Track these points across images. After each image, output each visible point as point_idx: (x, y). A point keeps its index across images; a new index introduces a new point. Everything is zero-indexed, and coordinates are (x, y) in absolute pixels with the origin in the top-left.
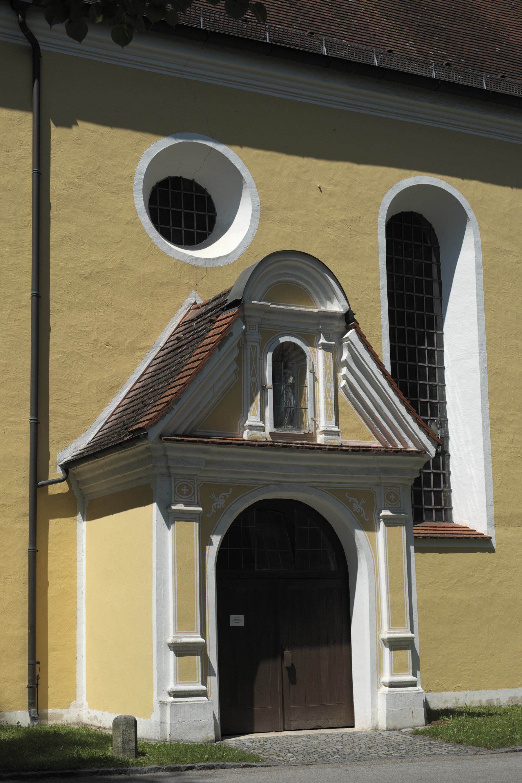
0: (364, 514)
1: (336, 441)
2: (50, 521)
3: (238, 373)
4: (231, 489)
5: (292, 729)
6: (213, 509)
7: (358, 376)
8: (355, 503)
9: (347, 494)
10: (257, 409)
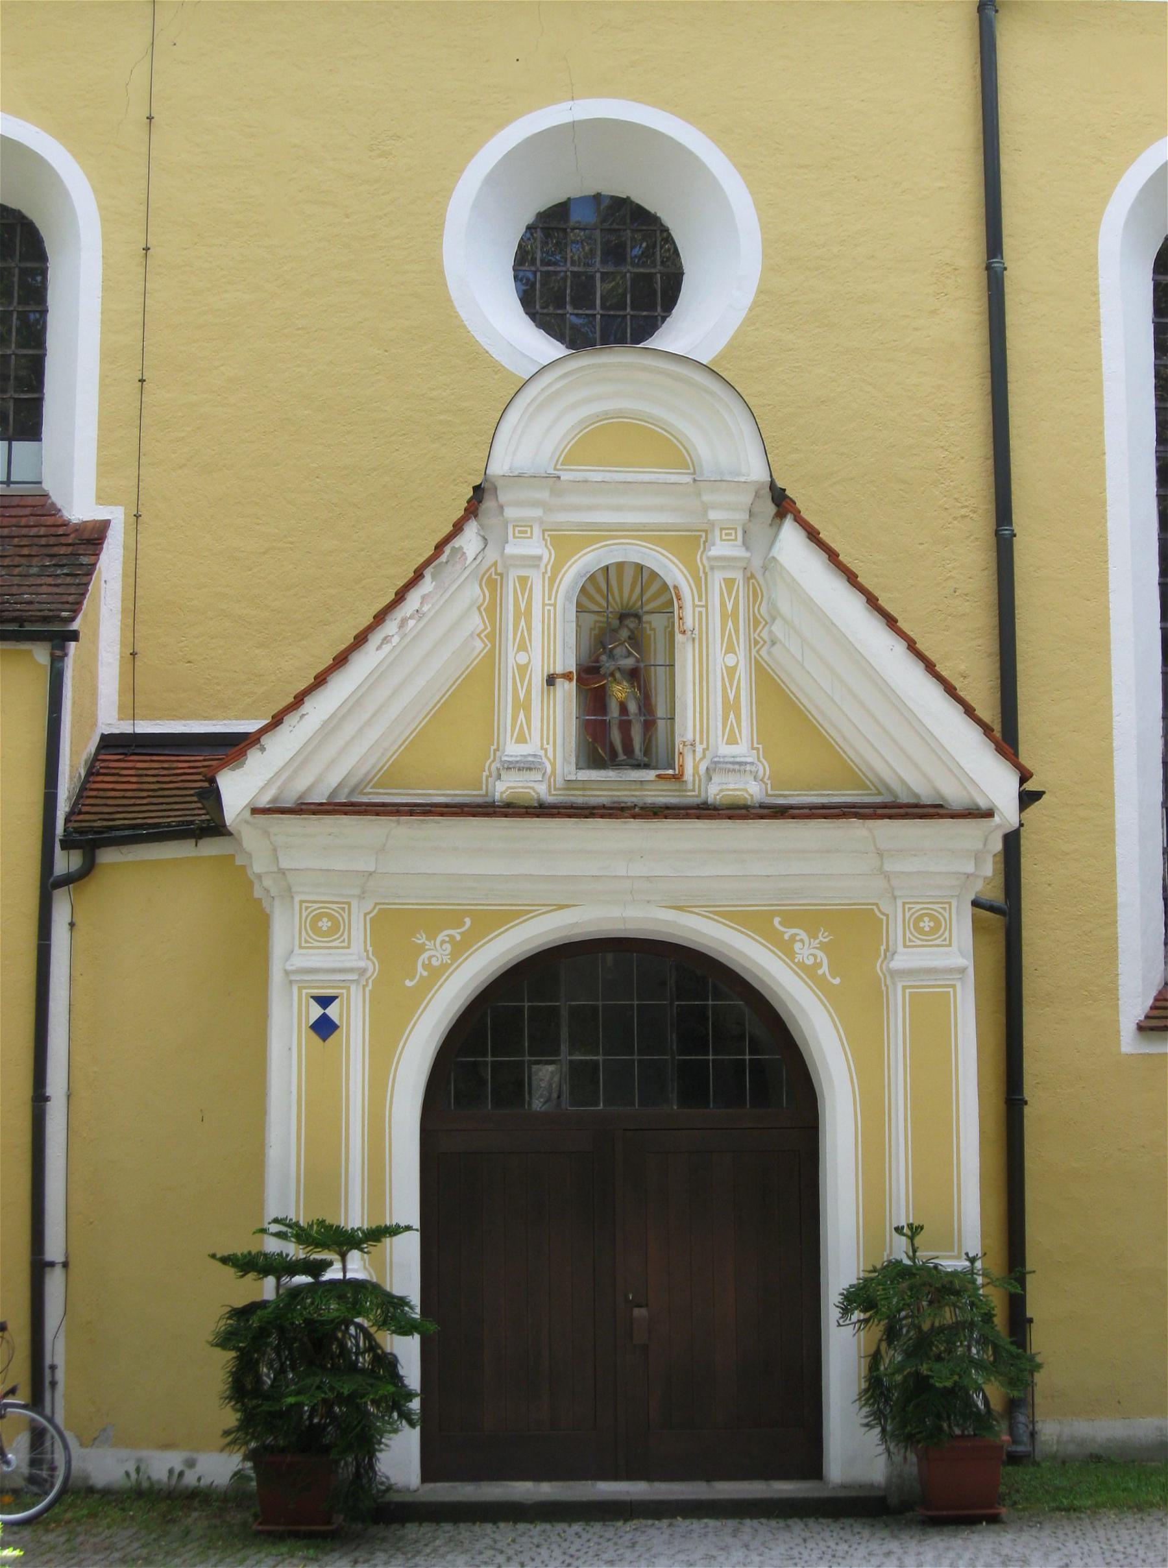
0: (824, 969)
3: (494, 636)
4: (468, 921)
7: (94, 676)
8: (802, 941)
9: (777, 920)
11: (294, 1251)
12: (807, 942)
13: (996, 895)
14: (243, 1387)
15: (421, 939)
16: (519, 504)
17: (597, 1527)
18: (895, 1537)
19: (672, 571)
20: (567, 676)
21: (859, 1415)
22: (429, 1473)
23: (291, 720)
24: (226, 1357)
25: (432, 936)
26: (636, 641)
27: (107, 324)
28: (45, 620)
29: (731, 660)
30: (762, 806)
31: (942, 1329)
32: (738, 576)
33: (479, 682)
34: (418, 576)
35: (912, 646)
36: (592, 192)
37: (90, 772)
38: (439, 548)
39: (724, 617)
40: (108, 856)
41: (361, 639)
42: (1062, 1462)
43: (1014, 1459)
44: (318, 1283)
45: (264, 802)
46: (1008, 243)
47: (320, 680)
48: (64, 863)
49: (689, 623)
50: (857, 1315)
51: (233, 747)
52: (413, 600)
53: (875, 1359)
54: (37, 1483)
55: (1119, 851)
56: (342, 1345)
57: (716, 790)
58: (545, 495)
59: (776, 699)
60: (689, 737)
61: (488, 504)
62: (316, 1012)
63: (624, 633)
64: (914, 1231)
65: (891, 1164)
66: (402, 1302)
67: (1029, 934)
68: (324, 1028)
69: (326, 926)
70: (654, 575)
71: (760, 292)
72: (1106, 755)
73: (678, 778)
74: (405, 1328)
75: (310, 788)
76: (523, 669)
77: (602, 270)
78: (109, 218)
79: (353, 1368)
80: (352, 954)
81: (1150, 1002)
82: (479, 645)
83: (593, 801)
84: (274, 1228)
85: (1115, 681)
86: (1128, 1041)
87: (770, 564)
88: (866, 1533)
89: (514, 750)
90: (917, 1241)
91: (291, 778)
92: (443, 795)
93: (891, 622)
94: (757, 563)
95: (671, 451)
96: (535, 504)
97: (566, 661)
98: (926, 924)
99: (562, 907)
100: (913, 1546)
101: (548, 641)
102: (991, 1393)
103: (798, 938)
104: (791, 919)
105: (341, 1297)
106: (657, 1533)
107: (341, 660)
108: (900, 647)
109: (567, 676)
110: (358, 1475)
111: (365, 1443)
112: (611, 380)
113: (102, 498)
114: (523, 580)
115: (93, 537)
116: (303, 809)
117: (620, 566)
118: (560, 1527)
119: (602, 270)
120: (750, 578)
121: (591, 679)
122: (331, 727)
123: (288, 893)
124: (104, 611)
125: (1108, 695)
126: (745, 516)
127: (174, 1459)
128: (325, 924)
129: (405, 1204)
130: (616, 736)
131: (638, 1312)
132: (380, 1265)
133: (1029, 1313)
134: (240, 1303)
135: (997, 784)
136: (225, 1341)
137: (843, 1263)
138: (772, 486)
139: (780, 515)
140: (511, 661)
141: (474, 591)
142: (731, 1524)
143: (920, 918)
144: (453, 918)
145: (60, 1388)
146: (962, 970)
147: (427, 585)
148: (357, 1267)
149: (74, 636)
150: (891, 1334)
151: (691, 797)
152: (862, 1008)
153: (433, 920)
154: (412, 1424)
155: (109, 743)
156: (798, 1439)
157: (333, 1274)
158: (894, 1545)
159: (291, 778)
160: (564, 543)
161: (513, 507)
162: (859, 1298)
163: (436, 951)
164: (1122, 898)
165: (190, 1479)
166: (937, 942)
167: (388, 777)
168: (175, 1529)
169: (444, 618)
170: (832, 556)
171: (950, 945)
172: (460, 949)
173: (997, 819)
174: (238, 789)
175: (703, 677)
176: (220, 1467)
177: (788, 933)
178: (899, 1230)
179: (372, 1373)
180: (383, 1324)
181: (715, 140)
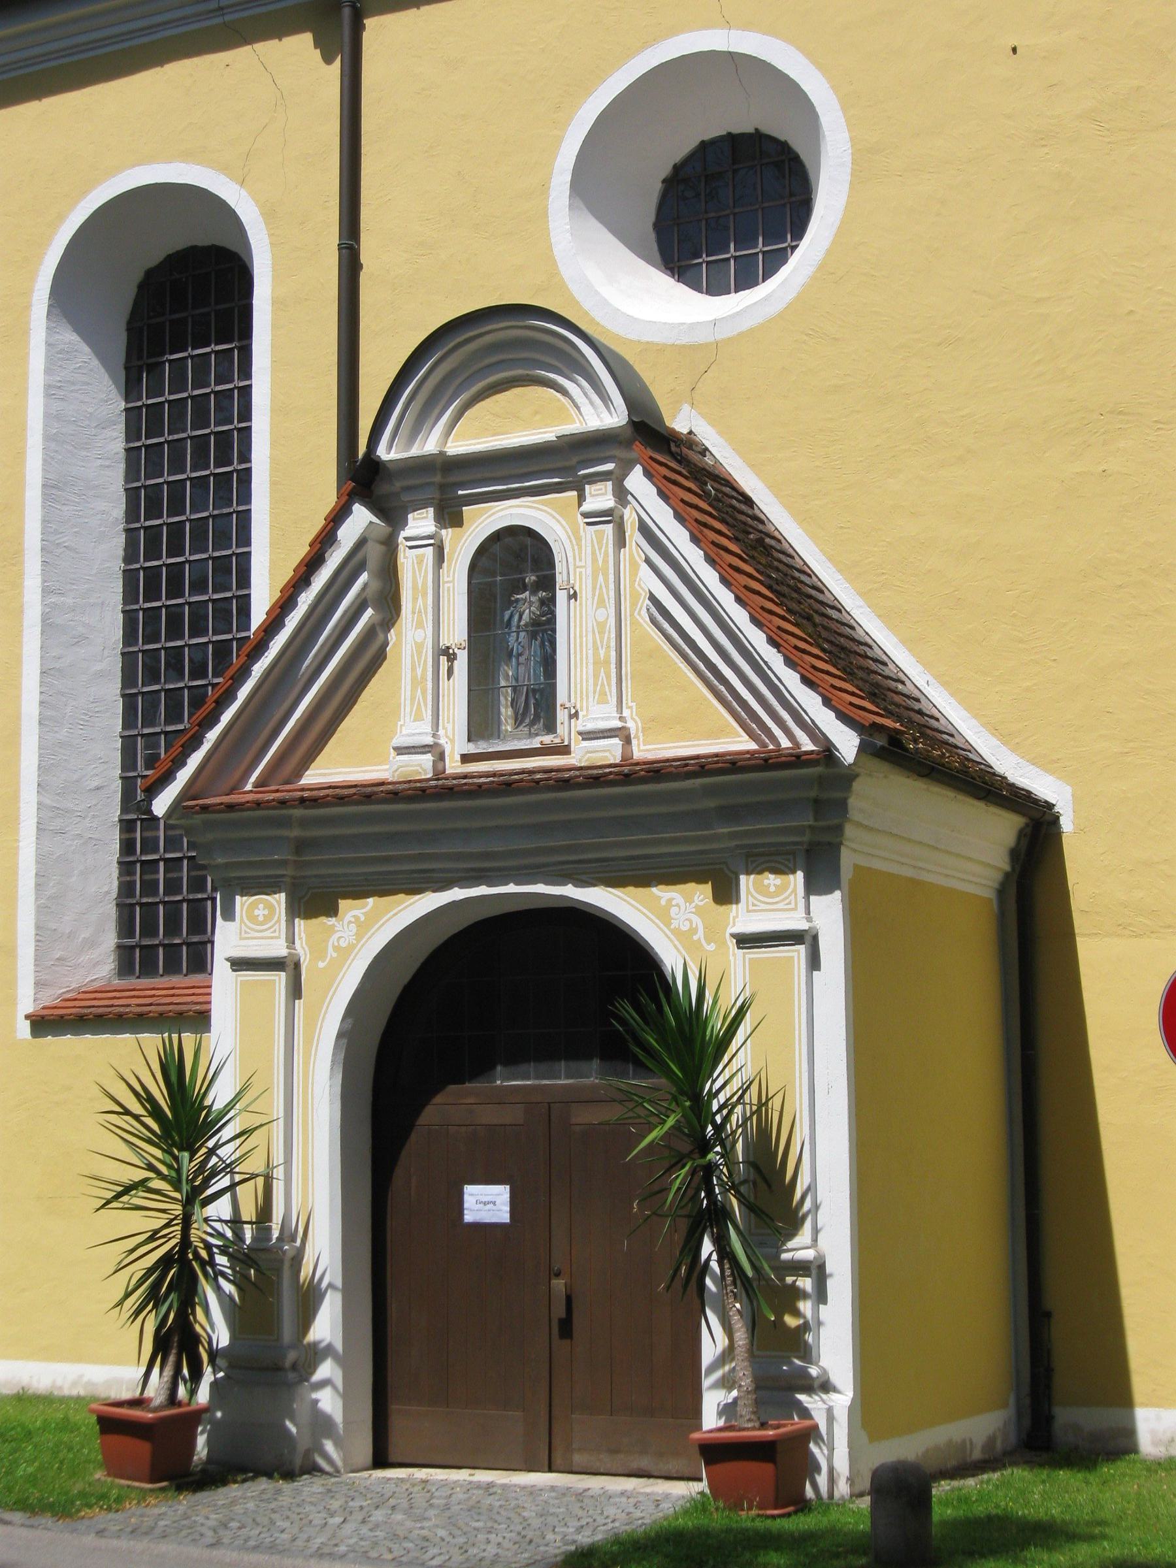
0: (700, 934)
1: (607, 754)
2: (743, 878)
5: (574, 1469)
6: (330, 949)
10: (426, 705)
12: (683, 908)
92: (321, 775)
103: (674, 903)
140: (410, 638)
166: (781, 906)
171: (241, 939)
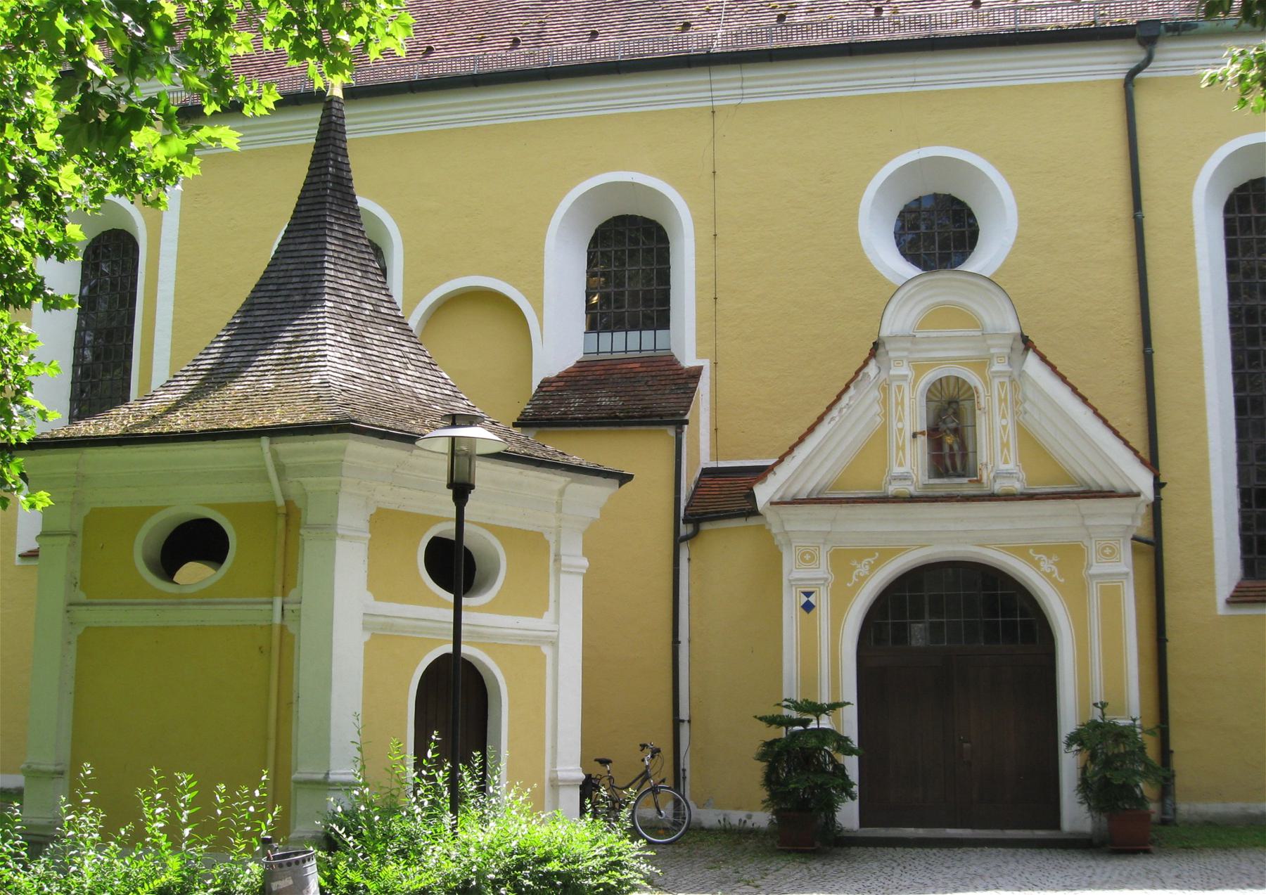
0: (1056, 575)
9: (1031, 551)
11: (795, 715)
13: (1147, 533)
14: (771, 780)
15: (854, 563)
16: (896, 350)
17: (945, 851)
18: (1094, 858)
19: (974, 379)
20: (922, 433)
21: (1077, 798)
22: (863, 824)
23: (788, 459)
24: (763, 765)
25: (860, 561)
26: (957, 414)
27: (698, 272)
28: (673, 415)
29: (1004, 422)
30: (1022, 494)
31: (1117, 755)
32: (1007, 380)
33: (879, 439)
34: (847, 387)
35: (1096, 412)
36: (931, 192)
37: (696, 487)
38: (857, 373)
39: (1000, 400)
40: (706, 527)
41: (820, 419)
42: (1190, 824)
43: (1164, 822)
44: (806, 730)
45: (776, 499)
46: (1145, 204)
47: (802, 440)
48: (685, 530)
49: (983, 405)
50: (1075, 747)
51: (761, 473)
52: (845, 399)
53: (1084, 769)
54: (677, 825)
55: (1214, 511)
56: (818, 759)
57: (998, 487)
58: (909, 345)
59: (1028, 441)
60: (984, 461)
61: (881, 350)
62: (804, 599)
63: (951, 411)
64: (1104, 705)
65: (1095, 670)
66: (847, 739)
67: (1167, 554)
68: (808, 607)
69: (808, 558)
70: (964, 382)
71: (1018, 237)
72: (1206, 462)
73: (979, 481)
74: (850, 752)
75: (799, 492)
76: (901, 430)
77: (939, 230)
78: (697, 221)
79: (824, 771)
80: (821, 570)
81: (1232, 588)
82: (878, 419)
83: (937, 494)
84: (785, 703)
85: (1209, 424)
86: (1221, 609)
87: (1022, 374)
88: (1079, 857)
89: (897, 470)
90: (1105, 710)
91: (789, 487)
93: (1084, 400)
94: (1016, 373)
95: (970, 320)
96: (904, 349)
97: (922, 426)
98: (1108, 551)
99: (922, 546)
100: (1102, 863)
101: (912, 415)
102: (1146, 788)
104: (1038, 550)
105: (817, 736)
106: (974, 855)
107: (811, 429)
108: (1090, 413)
109: (922, 433)
110: (826, 823)
111: (830, 807)
112: (943, 287)
113: (699, 355)
114: (899, 387)
115: (695, 374)
116: (795, 502)
117: (947, 377)
118: (926, 850)
119: (939, 230)
120: (1012, 381)
121: (934, 434)
122: (827, 438)
123: (789, 543)
124: (702, 409)
125: (1205, 432)
126: (1007, 351)
127: (742, 815)
128: (807, 557)
129: (849, 692)
130: (948, 462)
131: (966, 745)
132: (837, 721)
133: (1172, 748)
134: (768, 740)
135: (1142, 480)
136: (762, 757)
137: (1069, 719)
138: (1022, 335)
139: (1027, 349)
141: (875, 393)
142: (1012, 851)
143: (1104, 548)
144: (870, 553)
145: (688, 780)
146: (1127, 574)
147: (852, 391)
148: (825, 722)
149: (687, 422)
150: (1093, 757)
151: (986, 490)
152: (1076, 594)
153: (861, 554)
154: (853, 799)
155: (706, 472)
156: (1046, 808)
157: (813, 725)
158: (1092, 863)
159: (789, 487)
160: (919, 368)
161: (893, 351)
162: (1073, 739)
163: (862, 569)
164: (1216, 535)
165: (749, 824)
167: (836, 485)
168: (740, 848)
169: (860, 409)
170: (1053, 368)
172: (874, 568)
173: (1142, 497)
174: (764, 493)
175: (991, 430)
176: (762, 819)
177: (1037, 557)
178: (1095, 705)
179: (833, 774)
180: (838, 749)
181: (992, 163)
